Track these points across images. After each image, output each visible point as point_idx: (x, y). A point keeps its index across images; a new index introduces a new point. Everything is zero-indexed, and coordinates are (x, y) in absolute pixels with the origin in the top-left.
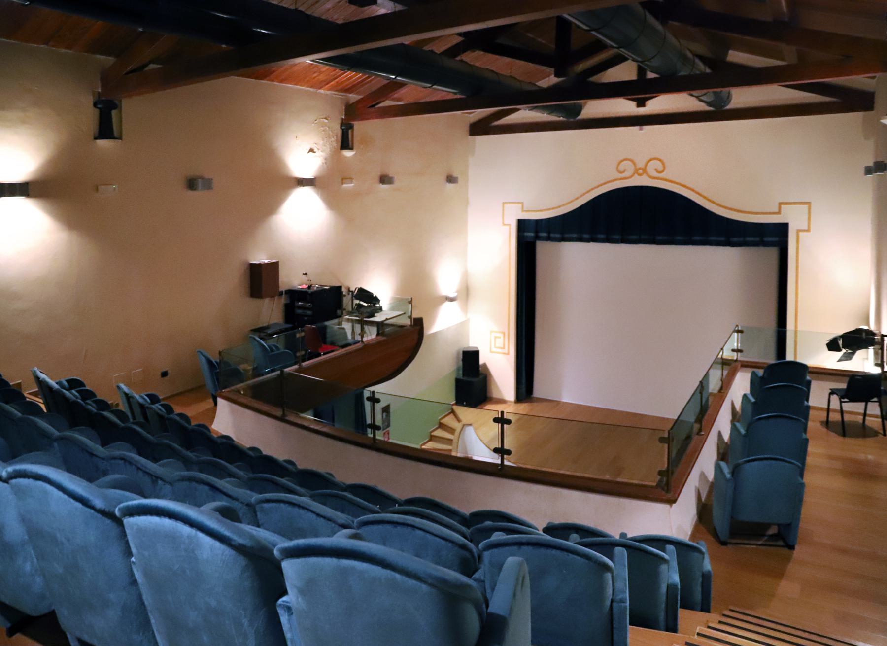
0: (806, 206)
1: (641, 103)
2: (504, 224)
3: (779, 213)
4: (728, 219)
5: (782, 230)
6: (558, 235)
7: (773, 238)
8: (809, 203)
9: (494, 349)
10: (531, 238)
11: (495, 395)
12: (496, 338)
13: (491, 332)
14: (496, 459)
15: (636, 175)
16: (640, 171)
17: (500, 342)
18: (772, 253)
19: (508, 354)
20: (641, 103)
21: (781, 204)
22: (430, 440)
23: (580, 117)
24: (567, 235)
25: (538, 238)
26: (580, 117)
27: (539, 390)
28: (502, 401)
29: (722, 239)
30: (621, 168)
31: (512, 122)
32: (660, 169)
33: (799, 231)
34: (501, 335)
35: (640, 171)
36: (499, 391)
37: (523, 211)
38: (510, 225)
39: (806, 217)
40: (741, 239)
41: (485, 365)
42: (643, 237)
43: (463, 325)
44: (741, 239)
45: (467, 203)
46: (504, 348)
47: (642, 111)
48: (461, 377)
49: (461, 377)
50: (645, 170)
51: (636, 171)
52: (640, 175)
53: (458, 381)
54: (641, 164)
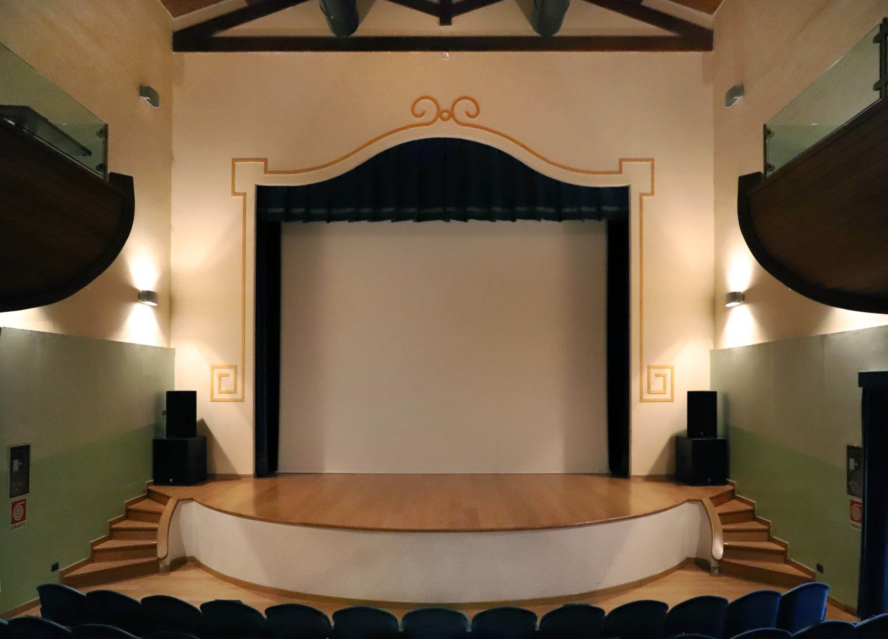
0: (649, 163)
1: (445, 20)
2: (234, 193)
3: (620, 172)
4: (558, 183)
5: (622, 195)
8: (652, 160)
9: (217, 396)
10: (279, 216)
11: (220, 470)
12: (220, 377)
13: (213, 368)
14: (657, 418)
15: (439, 119)
18: (594, 239)
20: (445, 20)
21: (621, 161)
22: (110, 538)
23: (357, 34)
24: (335, 211)
25: (290, 217)
26: (357, 34)
27: (287, 460)
28: (234, 478)
29: (552, 210)
30: (419, 108)
31: (248, 34)
32: (473, 110)
33: (641, 195)
34: (231, 372)
35: (445, 115)
36: (224, 458)
38: (244, 195)
39: (649, 177)
40: (575, 210)
41: (202, 421)
43: (167, 354)
44: (575, 210)
45: (169, 159)
46: (235, 392)
48: (163, 436)
49: (163, 436)
50: (451, 115)
51: (439, 114)
52: (445, 120)
54: (446, 105)
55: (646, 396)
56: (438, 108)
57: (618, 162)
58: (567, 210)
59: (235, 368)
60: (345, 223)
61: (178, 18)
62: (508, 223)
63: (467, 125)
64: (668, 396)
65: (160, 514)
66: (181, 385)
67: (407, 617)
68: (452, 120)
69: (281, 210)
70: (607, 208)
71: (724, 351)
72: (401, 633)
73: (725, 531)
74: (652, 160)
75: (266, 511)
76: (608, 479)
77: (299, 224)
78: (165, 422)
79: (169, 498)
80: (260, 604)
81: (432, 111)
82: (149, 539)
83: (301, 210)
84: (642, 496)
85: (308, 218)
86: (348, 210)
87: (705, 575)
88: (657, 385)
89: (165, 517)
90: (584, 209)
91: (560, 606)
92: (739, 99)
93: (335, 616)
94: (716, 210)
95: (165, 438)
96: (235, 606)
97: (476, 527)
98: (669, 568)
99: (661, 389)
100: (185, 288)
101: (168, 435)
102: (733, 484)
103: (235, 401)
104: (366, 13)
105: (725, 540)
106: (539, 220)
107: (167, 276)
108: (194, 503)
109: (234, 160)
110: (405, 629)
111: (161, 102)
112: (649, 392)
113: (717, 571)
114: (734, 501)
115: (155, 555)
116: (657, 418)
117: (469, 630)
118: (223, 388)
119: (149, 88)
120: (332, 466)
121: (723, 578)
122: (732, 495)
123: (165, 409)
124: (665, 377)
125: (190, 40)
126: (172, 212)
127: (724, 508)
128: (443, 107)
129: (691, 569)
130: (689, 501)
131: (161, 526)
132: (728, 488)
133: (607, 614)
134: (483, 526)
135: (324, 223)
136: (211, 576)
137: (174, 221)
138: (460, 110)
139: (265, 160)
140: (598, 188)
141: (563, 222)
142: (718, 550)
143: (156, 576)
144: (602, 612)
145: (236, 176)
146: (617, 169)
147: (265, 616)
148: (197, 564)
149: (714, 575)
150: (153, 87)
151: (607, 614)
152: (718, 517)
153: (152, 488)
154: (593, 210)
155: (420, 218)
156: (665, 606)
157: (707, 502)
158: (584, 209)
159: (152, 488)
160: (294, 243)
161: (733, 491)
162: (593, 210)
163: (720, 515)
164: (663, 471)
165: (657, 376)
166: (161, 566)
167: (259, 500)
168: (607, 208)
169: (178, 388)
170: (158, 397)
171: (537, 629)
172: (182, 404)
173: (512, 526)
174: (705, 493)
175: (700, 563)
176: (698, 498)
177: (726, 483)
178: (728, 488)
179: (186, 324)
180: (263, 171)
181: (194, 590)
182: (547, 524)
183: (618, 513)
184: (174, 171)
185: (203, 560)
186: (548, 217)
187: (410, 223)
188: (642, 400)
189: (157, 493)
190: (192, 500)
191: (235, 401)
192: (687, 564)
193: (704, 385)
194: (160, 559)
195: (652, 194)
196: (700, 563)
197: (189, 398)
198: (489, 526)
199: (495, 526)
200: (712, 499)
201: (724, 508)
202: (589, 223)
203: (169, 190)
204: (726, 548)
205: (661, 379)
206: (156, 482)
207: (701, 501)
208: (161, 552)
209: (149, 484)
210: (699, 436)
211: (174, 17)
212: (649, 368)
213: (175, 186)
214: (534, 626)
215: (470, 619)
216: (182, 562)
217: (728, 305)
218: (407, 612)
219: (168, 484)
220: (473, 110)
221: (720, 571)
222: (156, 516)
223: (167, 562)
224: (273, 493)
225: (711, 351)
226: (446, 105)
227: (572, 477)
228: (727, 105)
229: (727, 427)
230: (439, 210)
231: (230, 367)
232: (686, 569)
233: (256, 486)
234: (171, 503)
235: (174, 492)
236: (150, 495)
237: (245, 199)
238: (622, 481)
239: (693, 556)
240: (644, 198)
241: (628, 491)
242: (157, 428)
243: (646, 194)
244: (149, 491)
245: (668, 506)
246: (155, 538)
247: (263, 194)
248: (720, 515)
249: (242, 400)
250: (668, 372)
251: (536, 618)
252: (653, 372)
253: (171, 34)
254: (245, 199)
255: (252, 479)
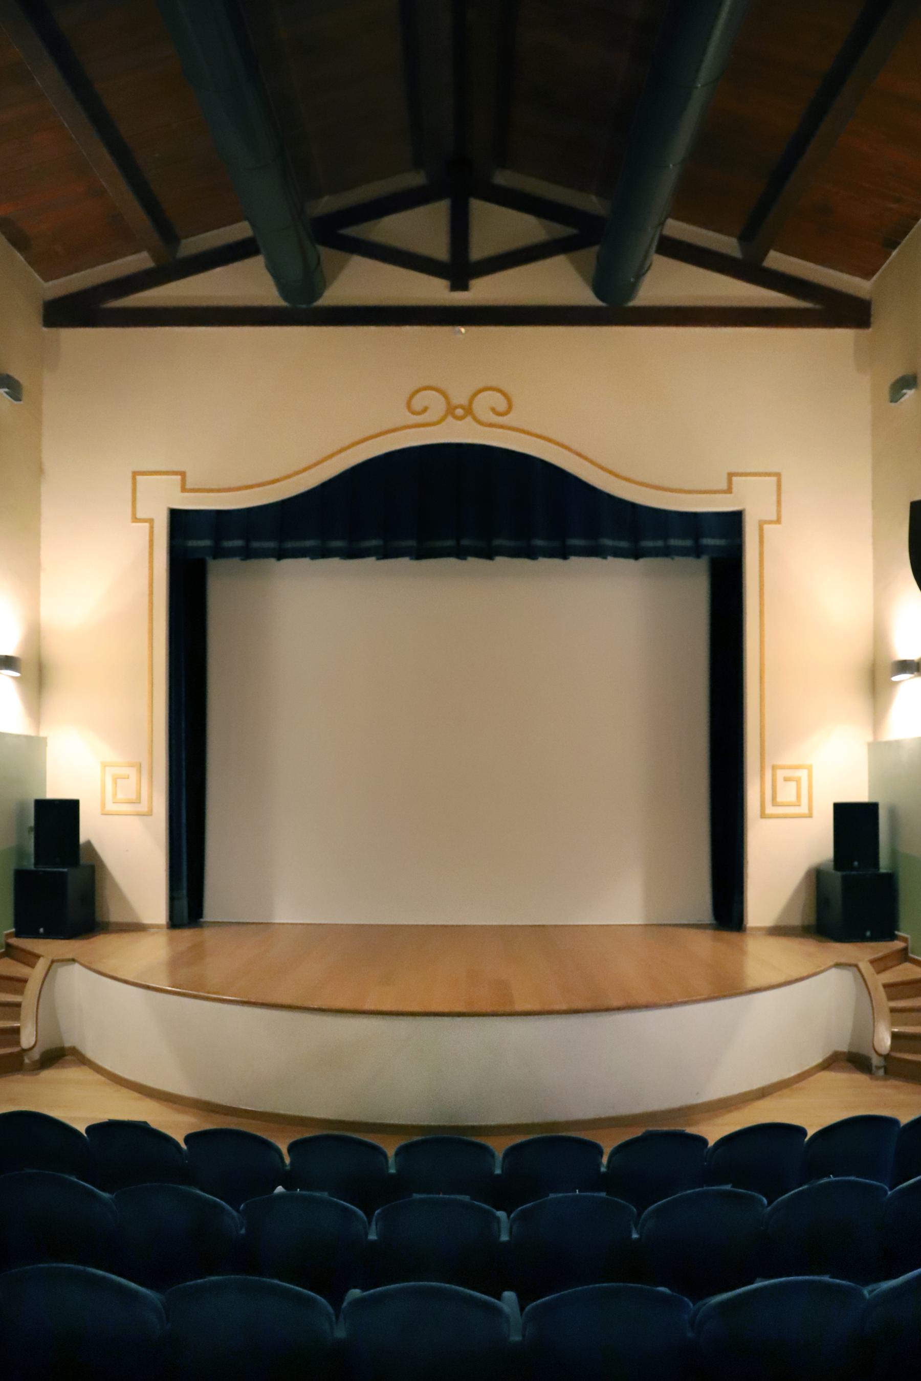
0: (774, 479)
1: (459, 284)
2: (135, 519)
3: (729, 490)
4: (634, 506)
5: (732, 522)
6: (271, 544)
7: (715, 550)
8: (778, 475)
9: (111, 807)
10: (202, 553)
11: (115, 915)
12: (115, 780)
13: (105, 765)
14: (786, 844)
15: (450, 419)
16: (459, 412)
17: (128, 789)
19: (149, 813)
20: (459, 284)
24: (290, 545)
25: (219, 553)
28: (137, 928)
29: (624, 544)
30: (417, 404)
32: (502, 405)
34: (132, 773)
35: (459, 412)
36: (122, 899)
37: (184, 489)
38: (151, 521)
39: (774, 498)
40: (660, 543)
41: (89, 844)
42: (465, 542)
43: (33, 746)
44: (660, 543)
45: (39, 471)
46: (138, 801)
47: (460, 298)
48: (30, 864)
49: (30, 864)
50: (469, 410)
51: (451, 410)
53: (22, 878)
54: (460, 397)
55: (770, 810)
56: (448, 402)
57: (725, 476)
58: (648, 544)
59: (139, 767)
60: (305, 562)
61: (50, 283)
62: (557, 562)
63: (491, 425)
64: (804, 809)
65: (25, 981)
66: (55, 791)
67: (402, 1152)
68: (469, 419)
69: (207, 543)
70: (708, 541)
71: (889, 744)
72: (392, 1175)
73: (893, 1010)
74: (778, 475)
75: (187, 983)
76: (709, 932)
77: (234, 563)
78: (32, 841)
79: (38, 957)
80: (176, 1126)
81: (437, 405)
82: (8, 1019)
83: (238, 543)
84: (763, 956)
85: (248, 554)
86: (309, 543)
87: (861, 1078)
88: (787, 793)
89: (32, 988)
90: (673, 542)
91: (638, 1132)
92: (909, 393)
93: (292, 1148)
94: (874, 544)
95: (32, 867)
96: (140, 1130)
97: (508, 1009)
98: (806, 1068)
99: (793, 798)
100: (58, 650)
101: (36, 864)
102: (905, 940)
103: (139, 814)
104: (334, 278)
105: (893, 1023)
106: (605, 558)
107: (35, 634)
108: (77, 967)
109: (135, 474)
110: (398, 1171)
111: (25, 397)
112: (774, 803)
113: (881, 1072)
114: (907, 965)
115: (18, 1043)
116: (786, 844)
117: (498, 1171)
118: (120, 796)
119: (9, 377)
120: (287, 911)
121: (889, 1082)
122: (904, 956)
123: (32, 823)
124: (798, 781)
125: (68, 312)
126: (43, 545)
127: (890, 976)
128: (455, 401)
129: (841, 1069)
130: (838, 965)
131: (28, 999)
132: (898, 945)
133: (711, 1143)
134: (519, 1007)
135: (273, 561)
136: (103, 1078)
137: (46, 555)
138: (482, 405)
139: (183, 474)
140: (695, 515)
141: (642, 561)
142: (884, 1041)
143: (19, 1076)
144: (704, 1141)
145: (138, 495)
146: (724, 486)
147: (184, 1146)
148: (81, 1060)
149: (877, 1079)
150: (12, 374)
151: (711, 1143)
152: (881, 989)
153: (14, 941)
154: (688, 543)
155: (420, 554)
156: (801, 1131)
157: (865, 967)
158: (673, 542)
159: (14, 941)
160: (230, 589)
161: (905, 950)
162: (688, 543)
163: (886, 986)
164: (796, 920)
165: (786, 779)
166: (27, 1061)
167: (175, 964)
168: (708, 541)
169: (52, 793)
170: (21, 809)
171: (603, 1169)
172: (58, 820)
173: (564, 1007)
174: (862, 954)
175: (855, 1061)
176: (853, 962)
177: (892, 937)
178: (898, 945)
179: (59, 701)
180: (179, 489)
181: (77, 1103)
182: (615, 1004)
183: (728, 986)
184: (44, 488)
185: (90, 1054)
186: (619, 553)
187: (404, 563)
188: (763, 815)
189: (23, 950)
190: (73, 960)
191: (139, 814)
192: (833, 1062)
193: (859, 794)
194: (24, 1051)
195: (778, 521)
196: (855, 1061)
197: (68, 811)
198: (528, 1007)
199: (537, 1007)
200: (872, 962)
201: (890, 976)
202: (680, 561)
203: (37, 514)
204: (895, 1036)
205: (793, 785)
206: (18, 934)
207: (856, 966)
208: (27, 1039)
209: (8, 936)
210: (853, 869)
211: (46, 279)
212: (774, 768)
213: (48, 510)
214: (599, 1164)
215: (499, 1155)
216: (57, 1056)
217: (895, 678)
218: (403, 1141)
219: (36, 935)
220: (502, 405)
221: (886, 1072)
222: (19, 983)
223: (36, 1055)
224: (197, 954)
225: (869, 744)
226: (460, 397)
227: (657, 929)
228: (892, 401)
229: (894, 854)
230: (450, 543)
231: (131, 765)
232: (833, 1070)
233: (171, 941)
234: (42, 965)
235: (48, 948)
236: (10, 952)
237: (152, 528)
238: (733, 936)
239: (844, 1048)
240: (766, 527)
241: (742, 951)
242: (20, 853)
243: (771, 522)
244: (8, 946)
245: (805, 974)
246: (17, 1018)
247: (181, 523)
248: (886, 986)
249: (149, 813)
250: (803, 774)
251: (601, 1153)
252: (781, 774)
253: (42, 302)
254: (152, 528)
255: (165, 930)
